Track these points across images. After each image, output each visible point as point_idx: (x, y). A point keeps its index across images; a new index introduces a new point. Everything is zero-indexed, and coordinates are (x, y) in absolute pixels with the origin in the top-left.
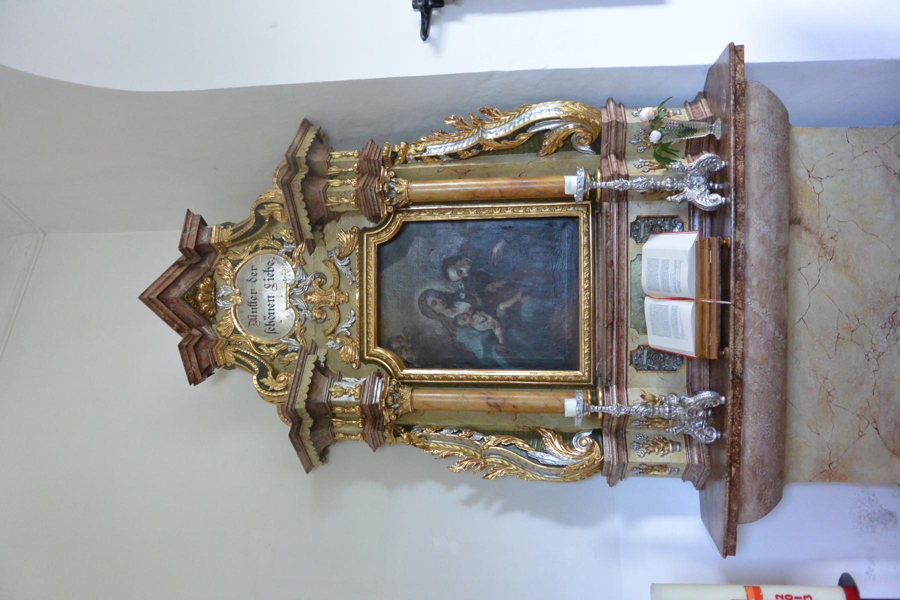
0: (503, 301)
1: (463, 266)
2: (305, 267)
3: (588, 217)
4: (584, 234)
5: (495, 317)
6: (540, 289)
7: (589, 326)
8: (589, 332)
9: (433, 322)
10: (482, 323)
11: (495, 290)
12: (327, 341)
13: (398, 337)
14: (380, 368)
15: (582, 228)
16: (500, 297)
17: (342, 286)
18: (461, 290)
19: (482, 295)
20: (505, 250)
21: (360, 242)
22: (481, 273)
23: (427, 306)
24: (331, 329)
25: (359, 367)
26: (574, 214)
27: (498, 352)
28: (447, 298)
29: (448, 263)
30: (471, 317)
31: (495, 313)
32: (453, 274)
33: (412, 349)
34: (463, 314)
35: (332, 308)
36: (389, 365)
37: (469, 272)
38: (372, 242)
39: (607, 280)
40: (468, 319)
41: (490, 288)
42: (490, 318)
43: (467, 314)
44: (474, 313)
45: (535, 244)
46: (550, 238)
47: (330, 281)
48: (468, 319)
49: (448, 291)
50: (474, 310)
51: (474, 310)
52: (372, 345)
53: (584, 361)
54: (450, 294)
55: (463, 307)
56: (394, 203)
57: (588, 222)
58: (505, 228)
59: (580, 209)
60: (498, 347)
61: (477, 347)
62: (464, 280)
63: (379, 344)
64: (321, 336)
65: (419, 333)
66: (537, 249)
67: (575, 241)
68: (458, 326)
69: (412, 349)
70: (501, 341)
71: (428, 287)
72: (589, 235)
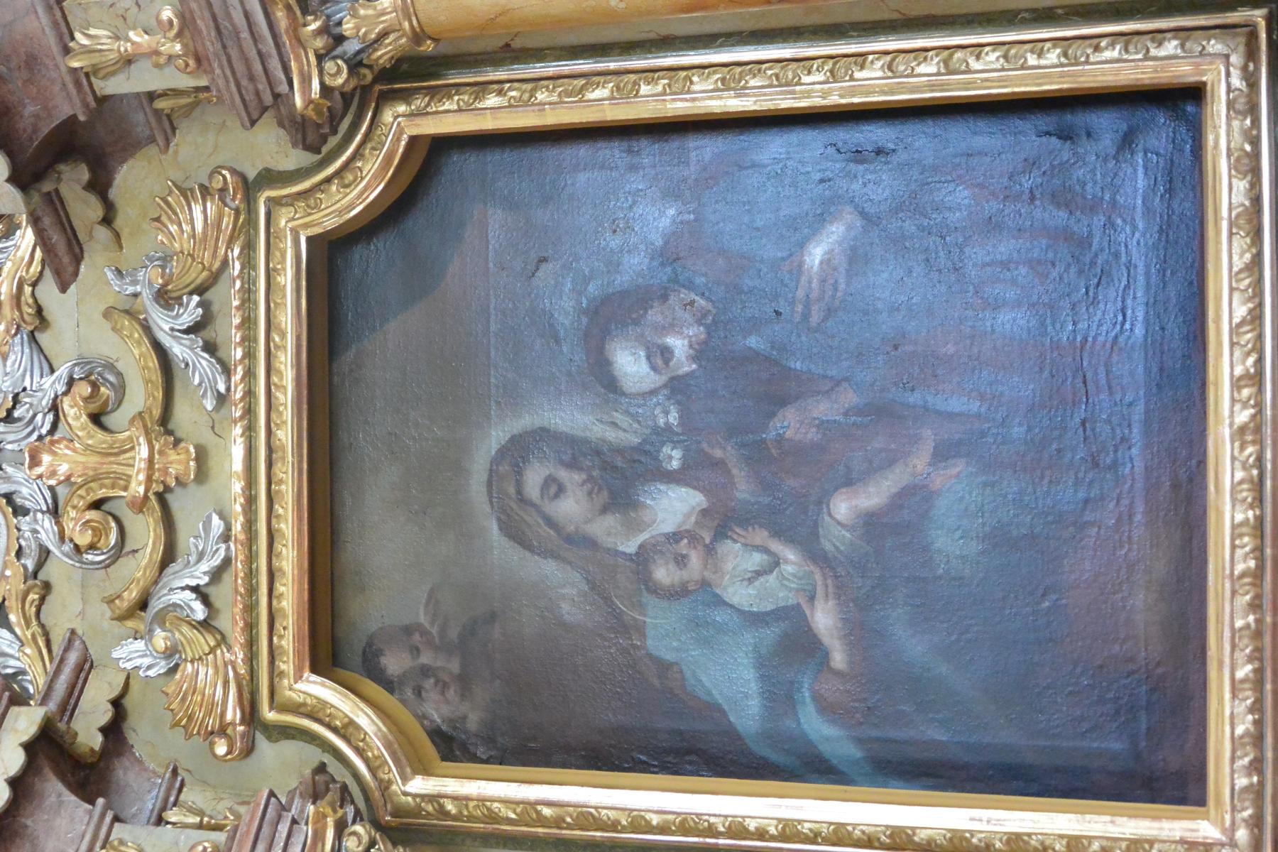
0: (849, 482)
1: (672, 327)
2: (43, 338)
3: (1253, 84)
4: (1235, 167)
5: (814, 554)
6: (1018, 431)
7: (1255, 606)
8: (1258, 634)
9: (550, 569)
10: (754, 575)
11: (813, 435)
12: (119, 641)
13: (408, 630)
14: (327, 758)
15: (1222, 132)
16: (827, 465)
17: (183, 414)
18: (665, 434)
19: (760, 455)
20: (856, 257)
21: (245, 231)
22: (753, 356)
23: (523, 500)
24: (133, 595)
25: (249, 750)
26: (1184, 72)
27: (826, 708)
28: (608, 467)
29: (614, 313)
30: (710, 550)
31: (815, 535)
32: (630, 364)
33: (464, 682)
34: (675, 537)
35: (140, 506)
36: (360, 752)
37: (700, 353)
38: (292, 231)
39: (78, 240)
40: (695, 559)
41: (791, 424)
42: (790, 555)
43: (693, 538)
44: (721, 533)
45: (992, 226)
46: (1063, 198)
47: (140, 395)
48: (695, 559)
49: (611, 435)
50: (723, 521)
51: (723, 521)
52: (287, 665)
53: (1227, 771)
54: (619, 451)
55: (673, 506)
56: (352, 47)
57: (1253, 109)
58: (858, 155)
59: (1215, 46)
60: (831, 688)
61: (731, 682)
62: (677, 387)
63: (326, 654)
64: (101, 614)
65: (492, 617)
66: (1005, 247)
67: (1182, 205)
68: (655, 590)
69: (464, 682)
70: (839, 659)
71: (525, 422)
72: (1256, 171)
